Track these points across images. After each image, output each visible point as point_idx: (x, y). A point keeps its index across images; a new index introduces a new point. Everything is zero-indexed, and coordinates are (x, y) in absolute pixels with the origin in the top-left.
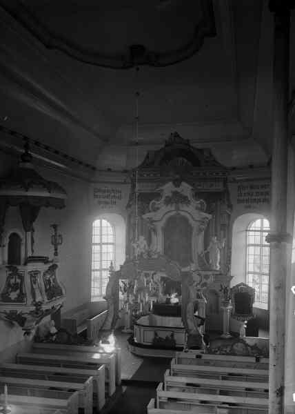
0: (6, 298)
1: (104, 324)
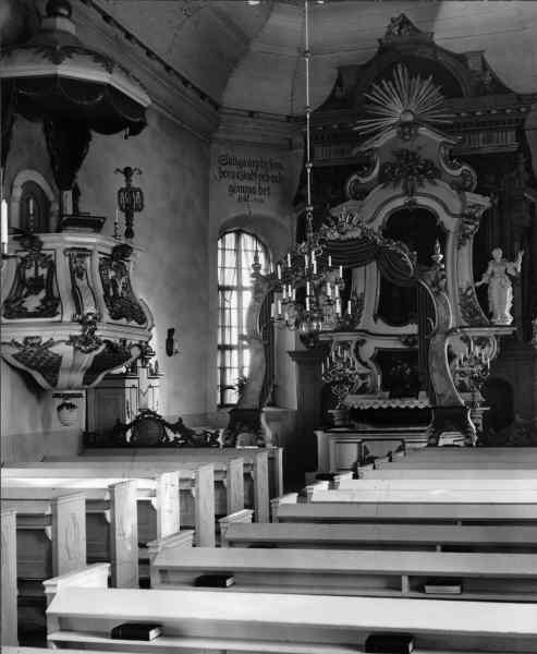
0: (14, 309)
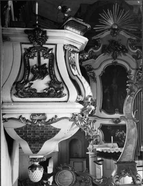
0: (22, 89)
1: (67, 149)
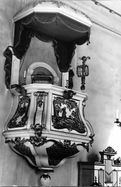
0: (12, 124)
